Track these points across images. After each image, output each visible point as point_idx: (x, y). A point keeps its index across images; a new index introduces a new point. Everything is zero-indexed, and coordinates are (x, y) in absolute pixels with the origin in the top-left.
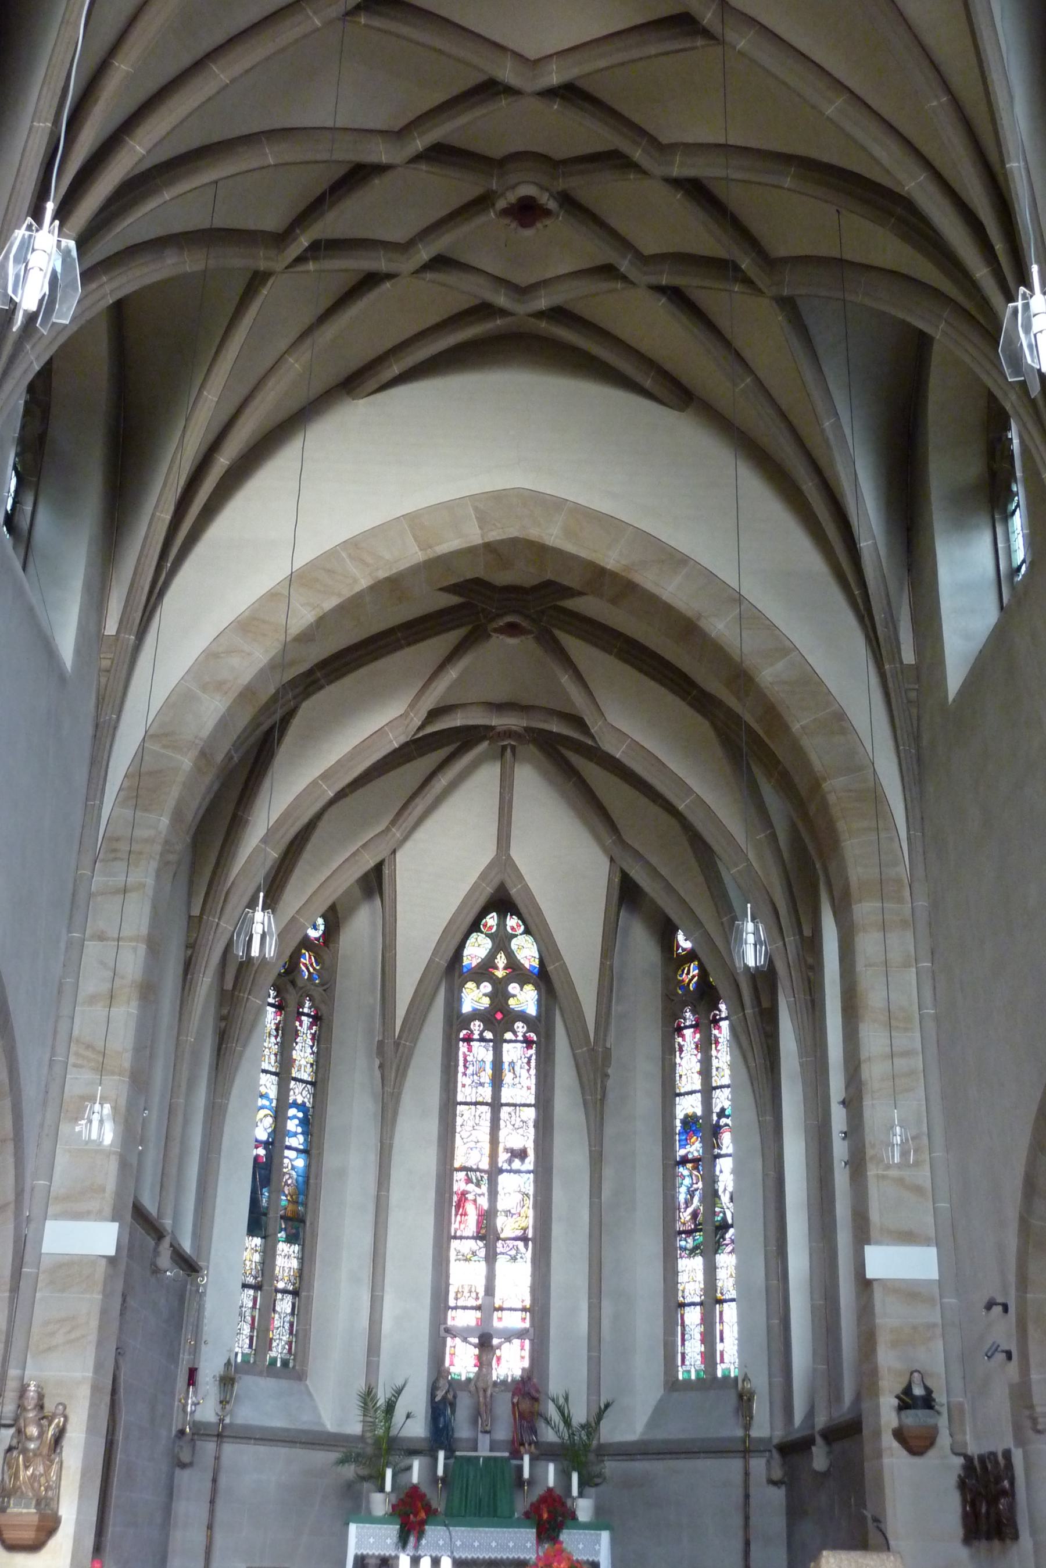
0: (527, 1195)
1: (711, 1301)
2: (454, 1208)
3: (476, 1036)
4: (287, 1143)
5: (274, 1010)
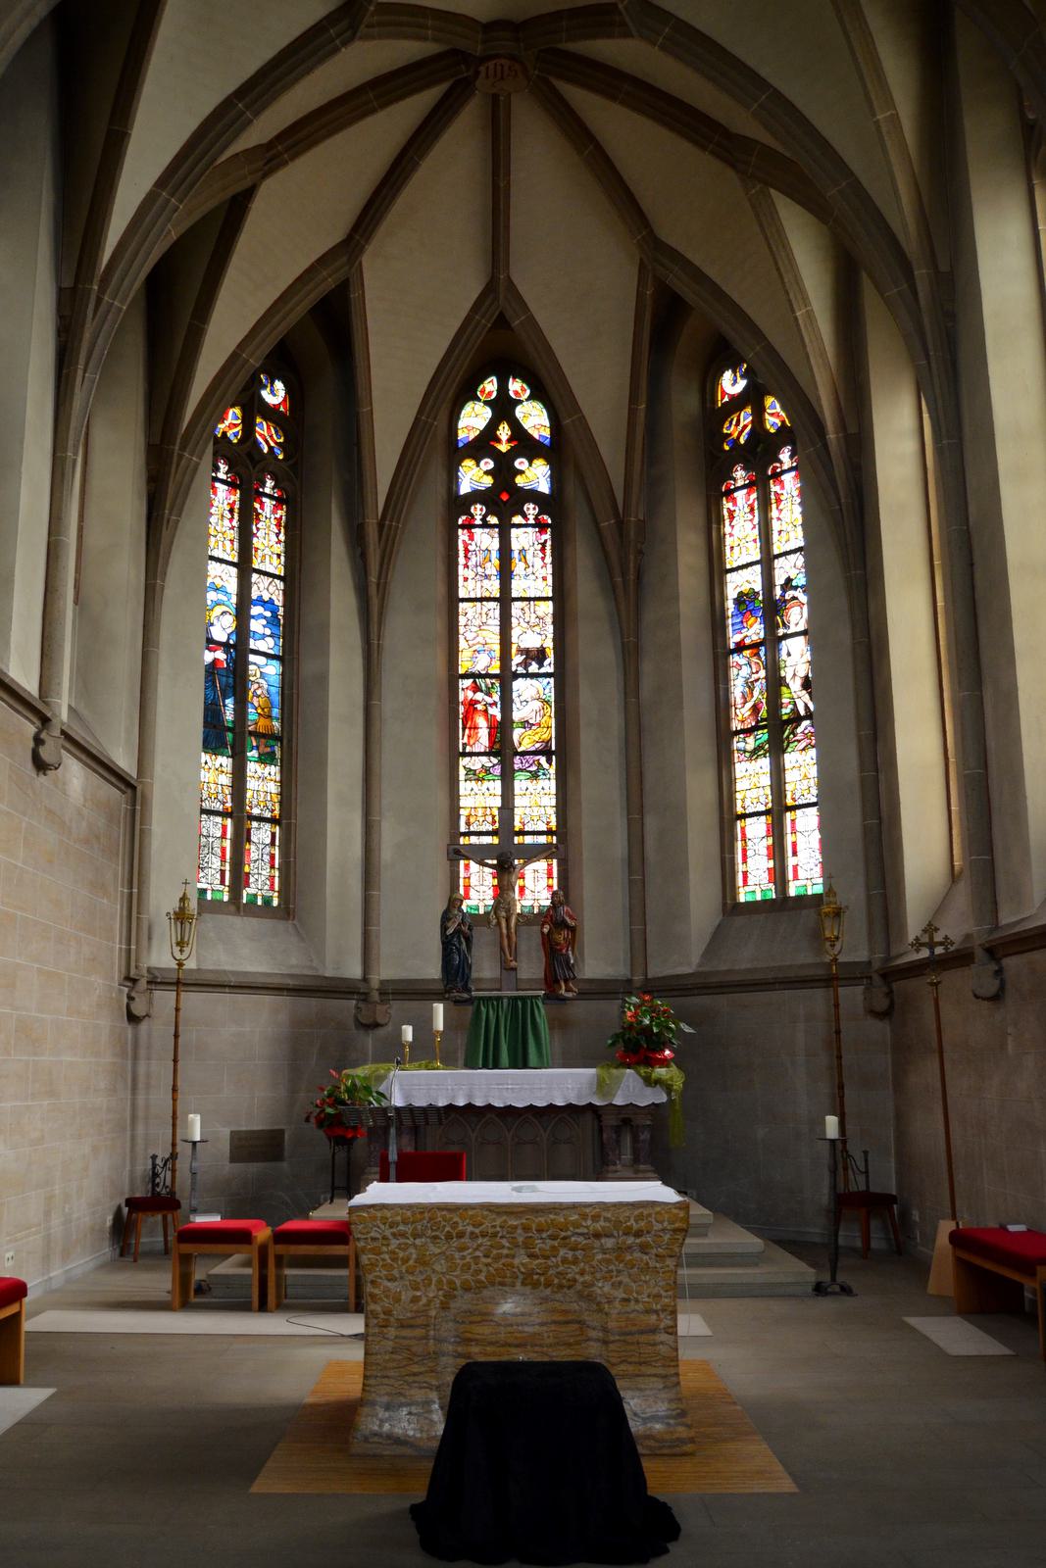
0: (547, 702)
1: (778, 811)
2: (460, 721)
4: (252, 646)
5: (226, 488)
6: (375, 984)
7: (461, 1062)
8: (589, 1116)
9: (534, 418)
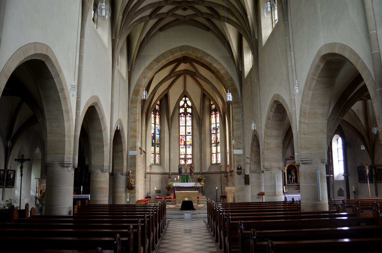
3: (182, 116)
6: (170, 173)
7: (181, 182)
8: (194, 188)
9: (189, 103)
